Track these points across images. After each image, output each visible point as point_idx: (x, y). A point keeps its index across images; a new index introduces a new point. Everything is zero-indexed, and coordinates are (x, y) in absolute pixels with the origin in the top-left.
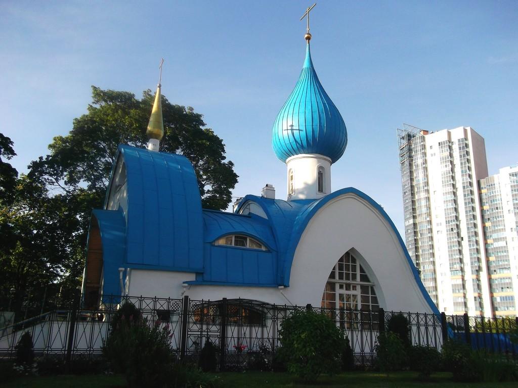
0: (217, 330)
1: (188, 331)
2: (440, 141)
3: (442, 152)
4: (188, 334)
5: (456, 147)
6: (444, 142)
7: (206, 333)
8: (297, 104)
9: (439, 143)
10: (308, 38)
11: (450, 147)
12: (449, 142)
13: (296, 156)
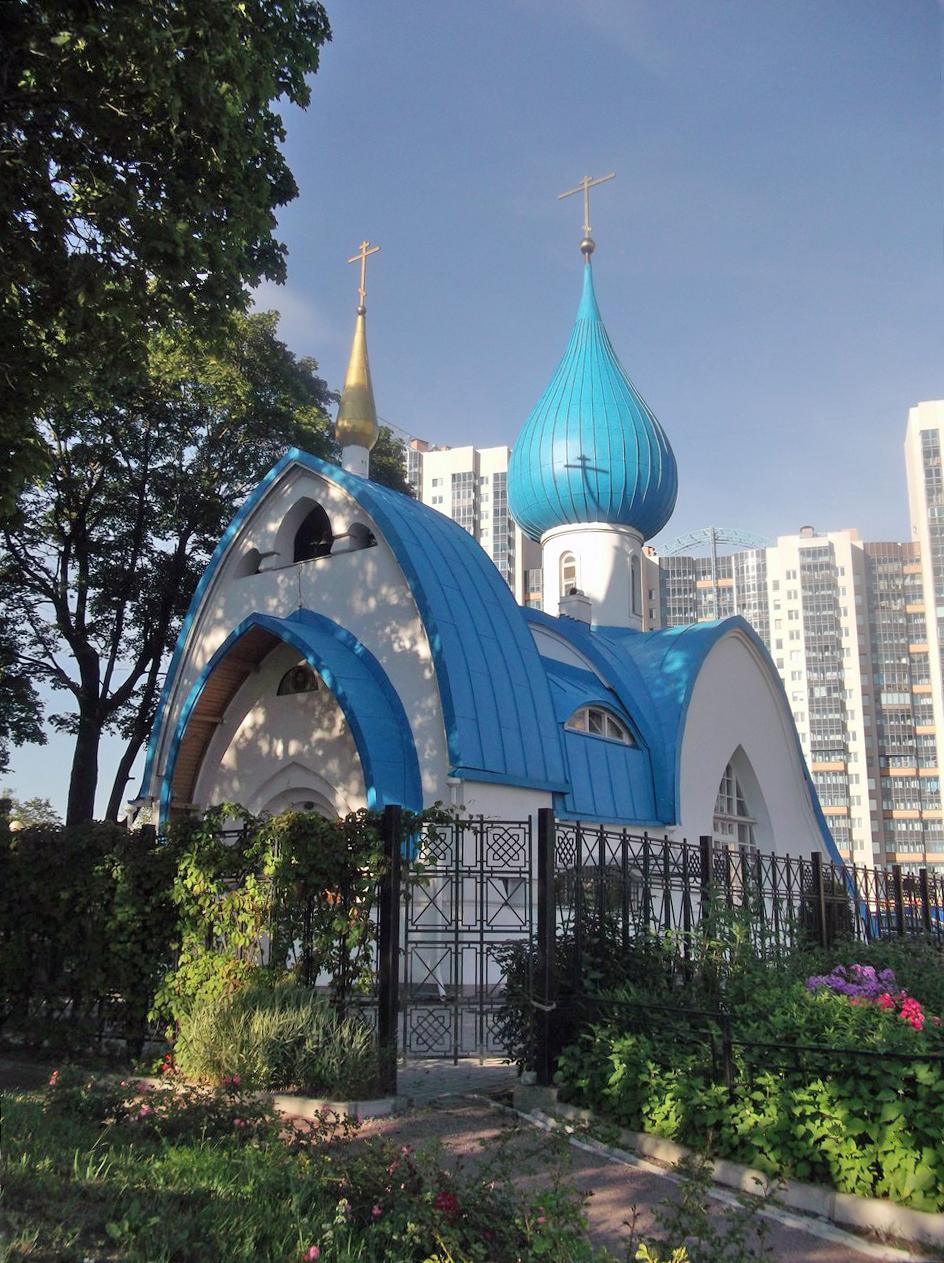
0: (440, 920)
1: (407, 931)
2: (456, 472)
3: (459, 497)
4: (407, 942)
5: (487, 489)
6: (464, 474)
7: (476, 937)
8: (564, 408)
9: (454, 476)
10: (588, 250)
11: (476, 489)
12: (475, 478)
13: (575, 526)
